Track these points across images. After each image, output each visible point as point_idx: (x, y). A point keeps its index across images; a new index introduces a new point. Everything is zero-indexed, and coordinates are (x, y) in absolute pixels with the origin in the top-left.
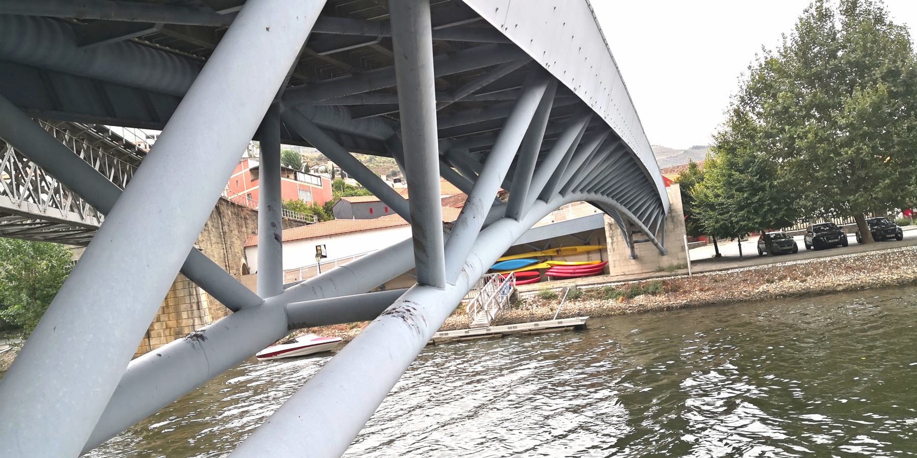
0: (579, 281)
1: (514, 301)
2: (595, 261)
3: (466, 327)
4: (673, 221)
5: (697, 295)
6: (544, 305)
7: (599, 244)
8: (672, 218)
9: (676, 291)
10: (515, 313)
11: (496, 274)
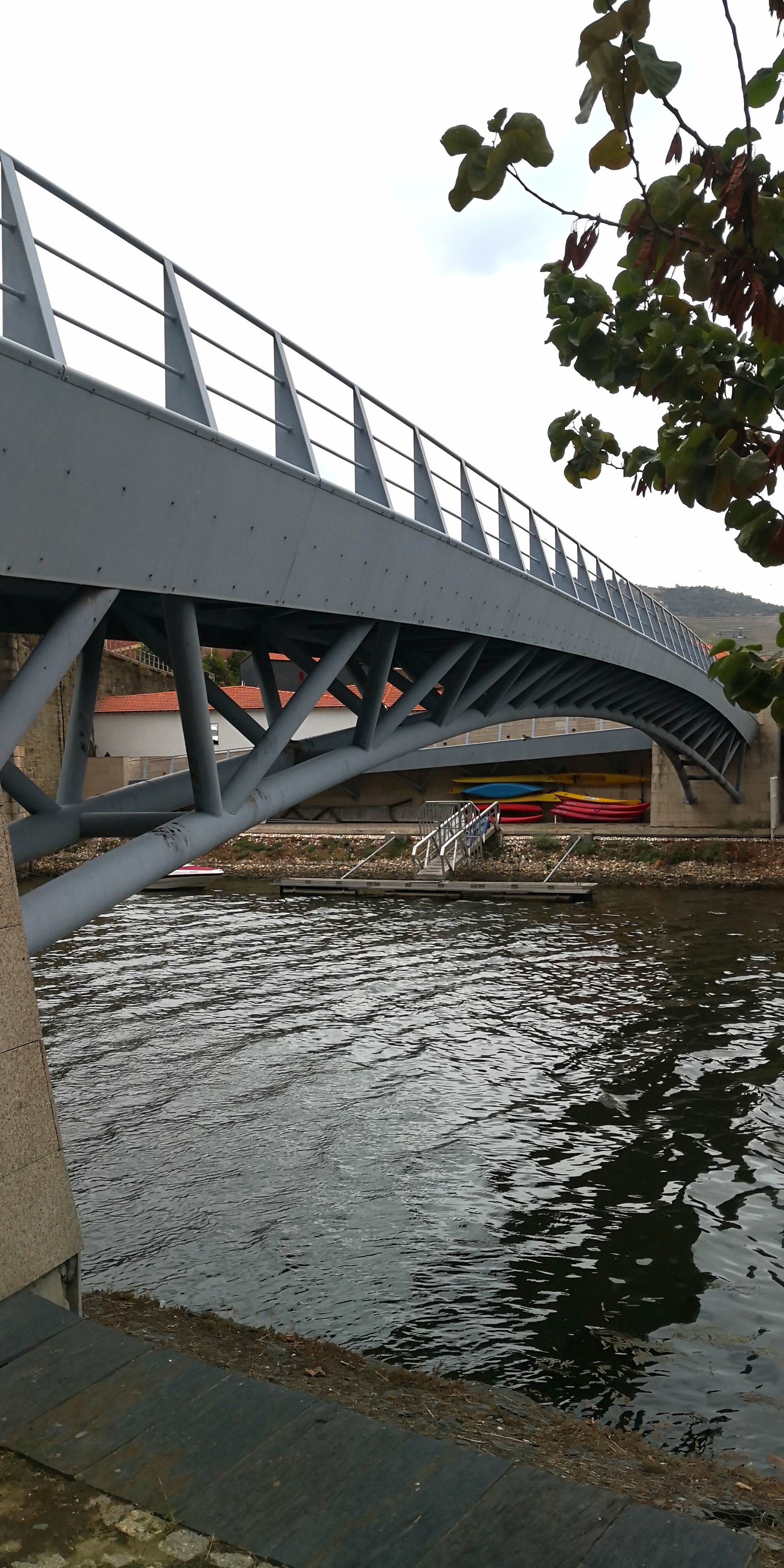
0: (600, 829)
1: (493, 846)
2: (633, 801)
3: (410, 876)
6: (537, 859)
7: (642, 774)
8: (760, 746)
11: (470, 803)
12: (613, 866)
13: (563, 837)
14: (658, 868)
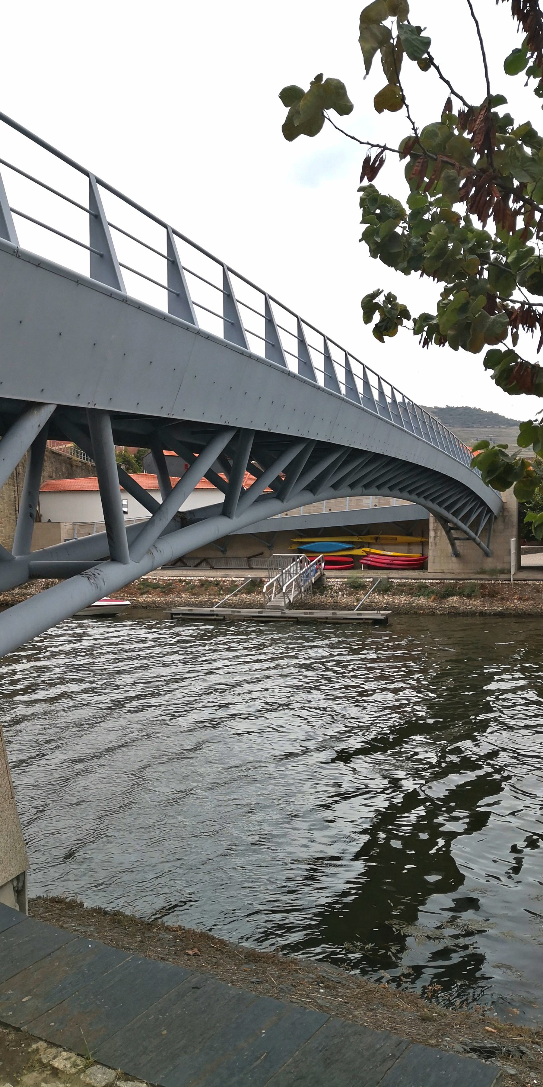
0: (393, 574)
2: (416, 554)
3: (262, 606)
4: (504, 521)
5: (515, 604)
6: (350, 594)
7: (423, 536)
8: (504, 517)
9: (494, 596)
10: (318, 598)
11: (304, 555)
12: (402, 600)
13: (368, 580)
14: (433, 601)
